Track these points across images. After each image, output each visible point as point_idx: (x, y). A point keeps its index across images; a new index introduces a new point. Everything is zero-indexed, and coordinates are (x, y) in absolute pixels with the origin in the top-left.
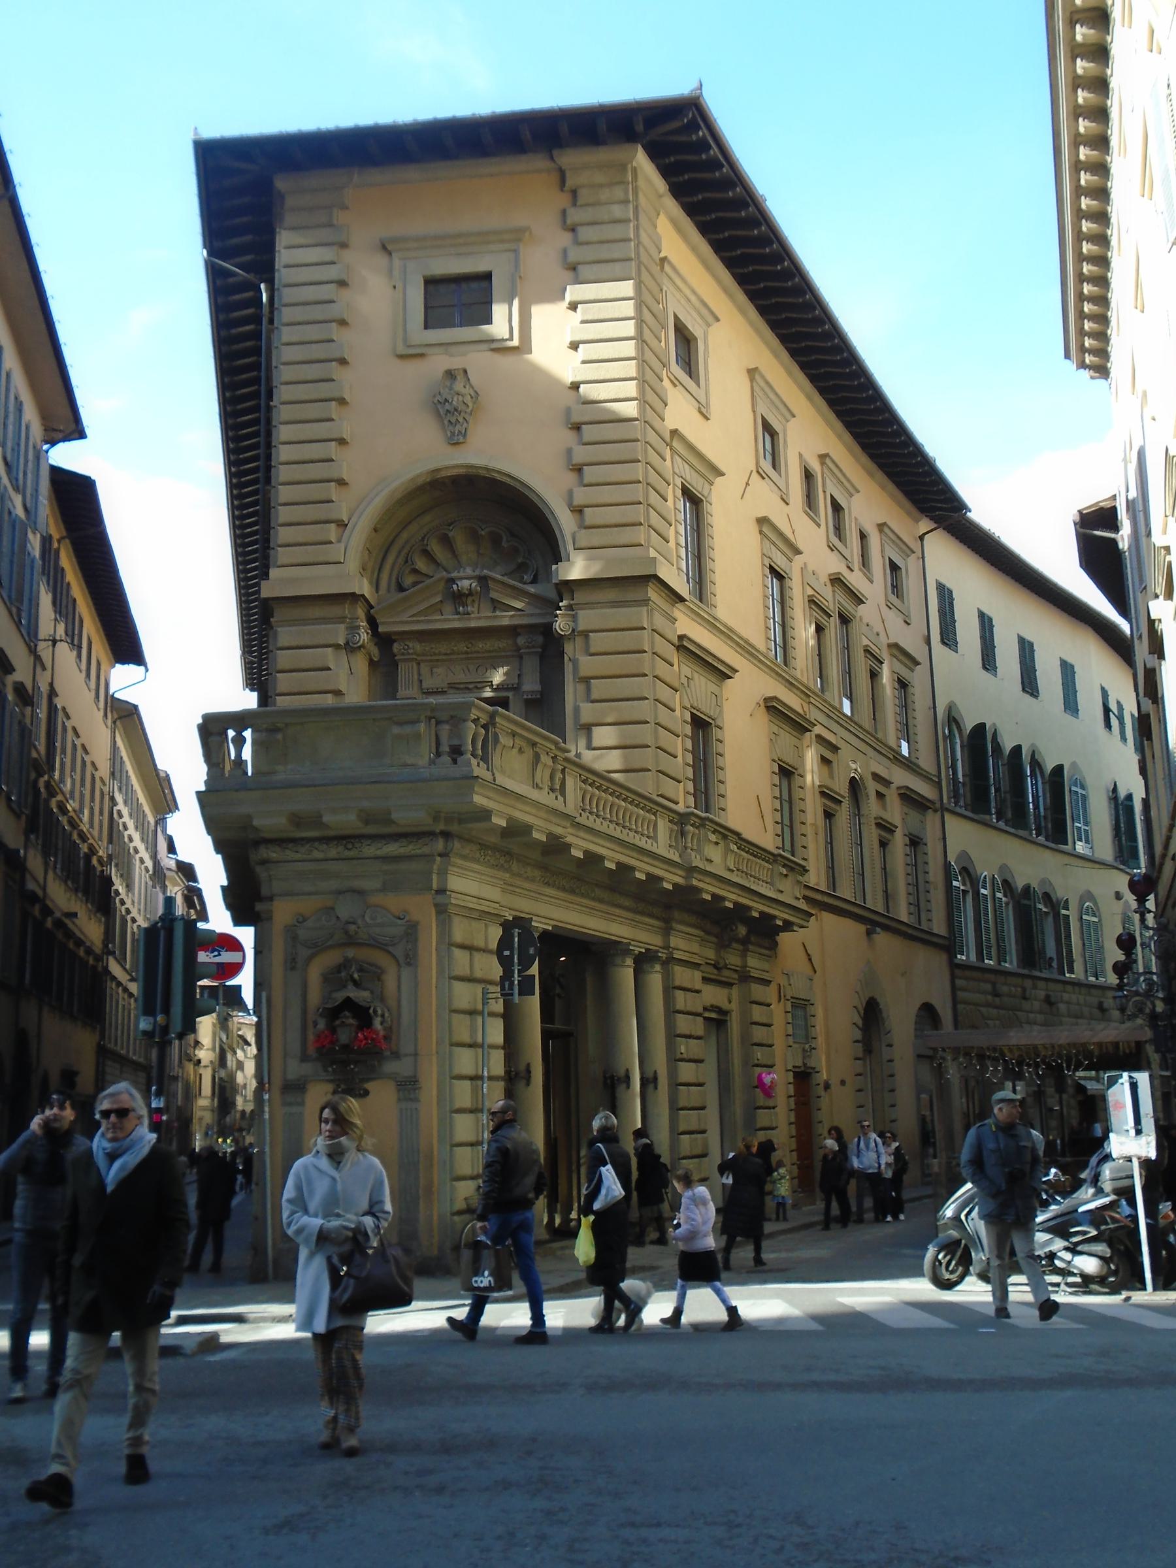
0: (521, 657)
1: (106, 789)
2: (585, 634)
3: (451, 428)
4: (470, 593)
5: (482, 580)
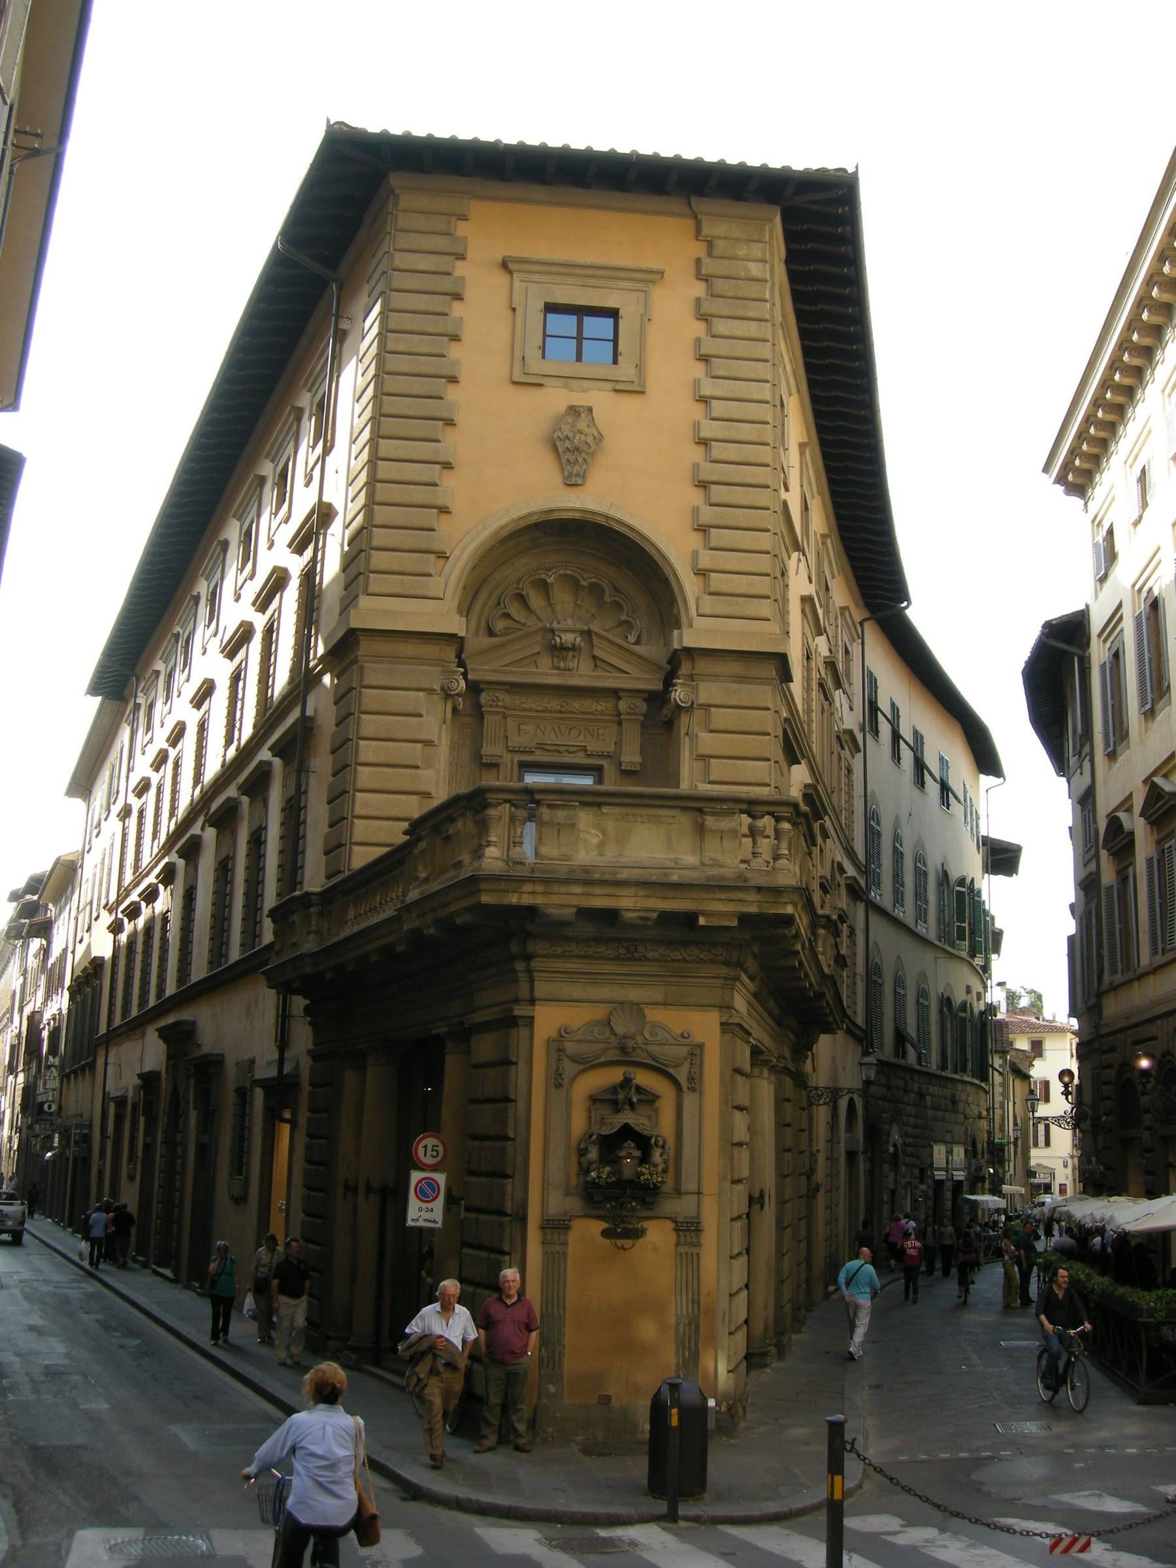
0: (620, 723)
2: (706, 707)
3: (568, 467)
4: (573, 648)
5: (588, 634)
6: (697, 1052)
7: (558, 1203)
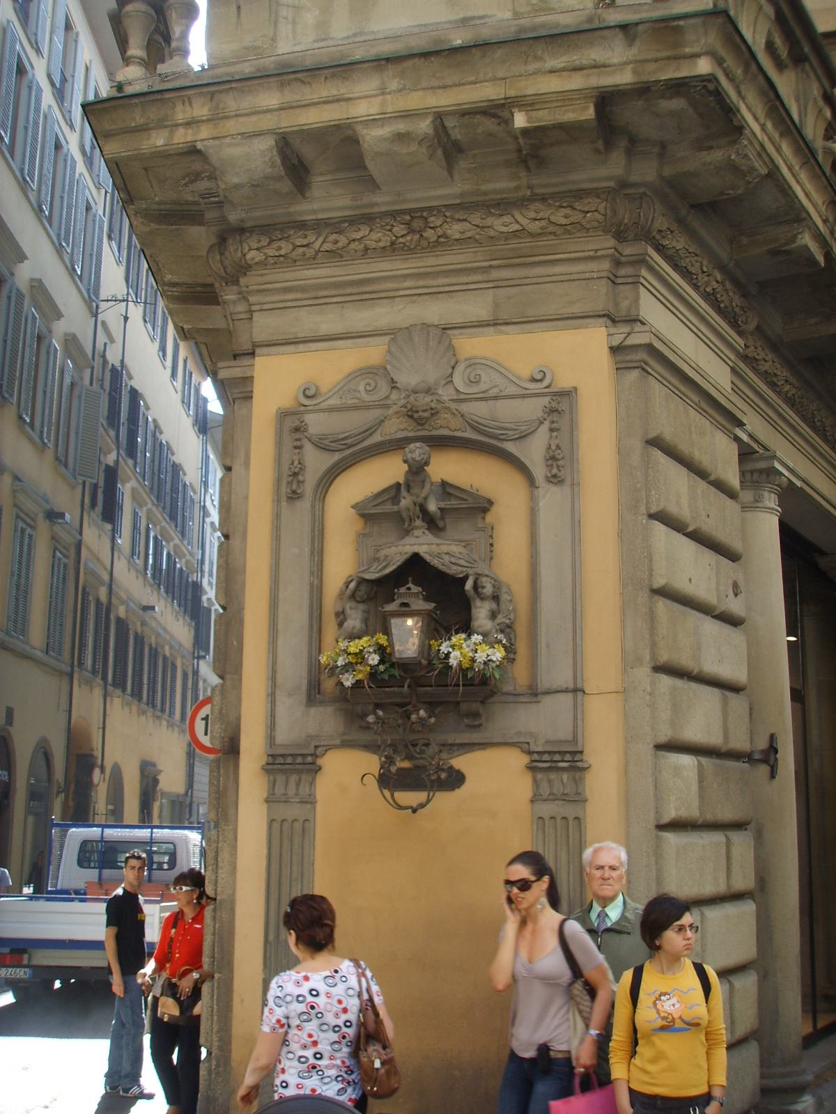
1: (196, 498)
6: (564, 406)
7: (299, 720)
